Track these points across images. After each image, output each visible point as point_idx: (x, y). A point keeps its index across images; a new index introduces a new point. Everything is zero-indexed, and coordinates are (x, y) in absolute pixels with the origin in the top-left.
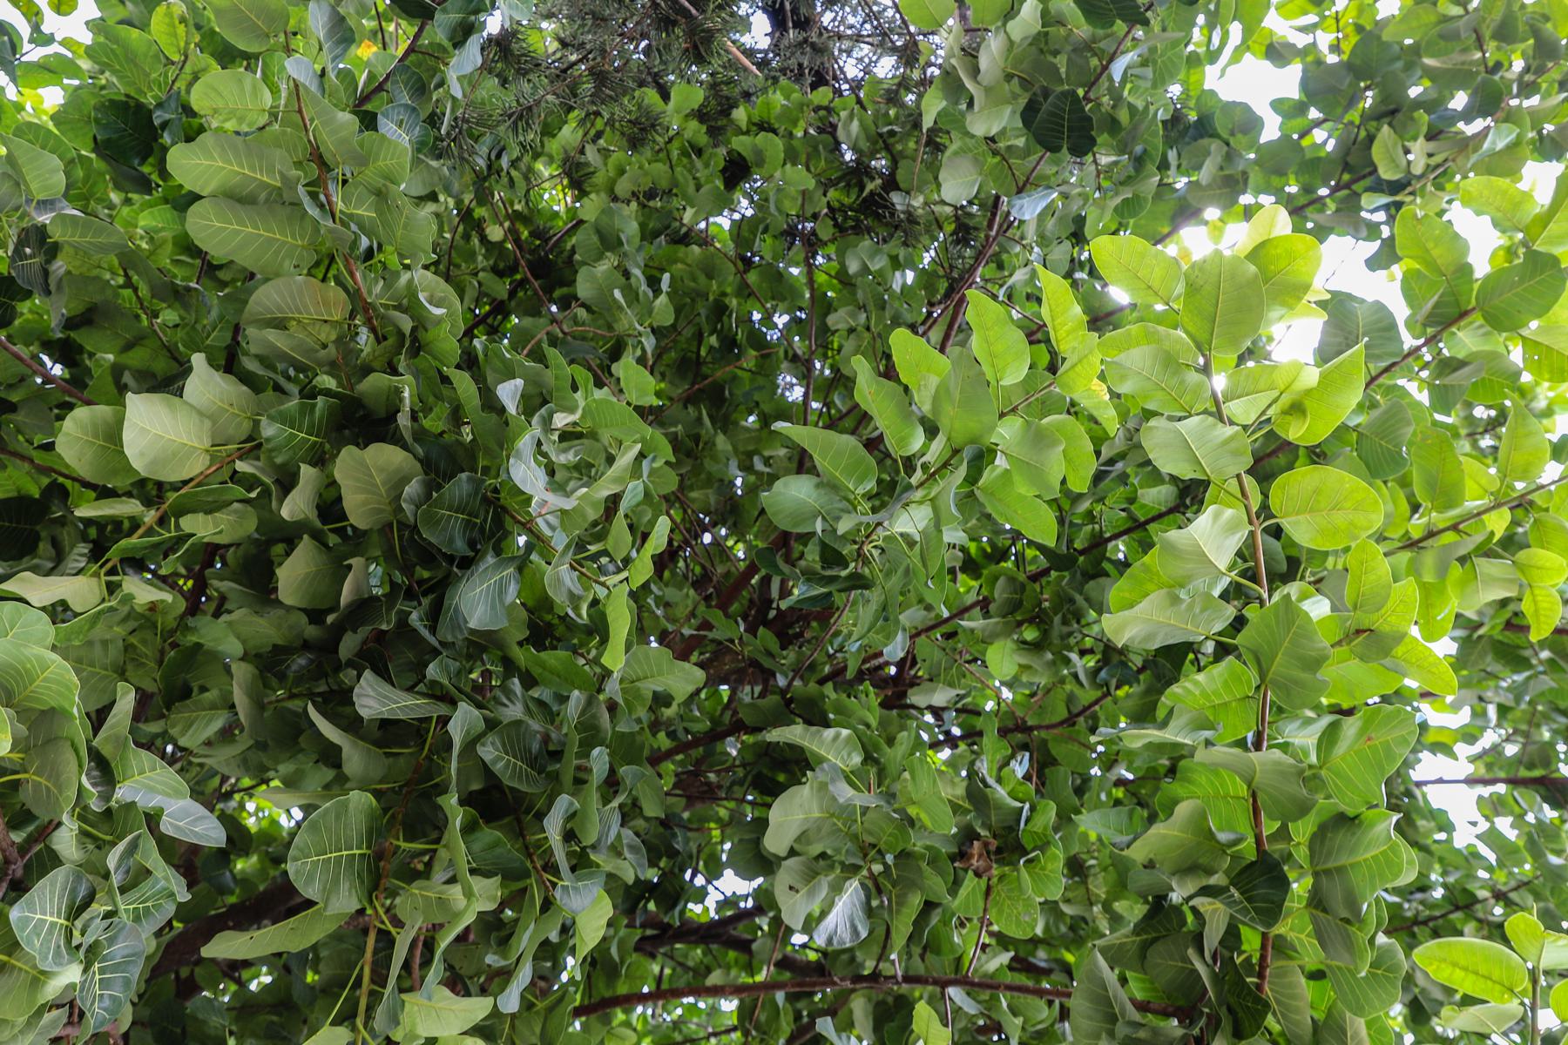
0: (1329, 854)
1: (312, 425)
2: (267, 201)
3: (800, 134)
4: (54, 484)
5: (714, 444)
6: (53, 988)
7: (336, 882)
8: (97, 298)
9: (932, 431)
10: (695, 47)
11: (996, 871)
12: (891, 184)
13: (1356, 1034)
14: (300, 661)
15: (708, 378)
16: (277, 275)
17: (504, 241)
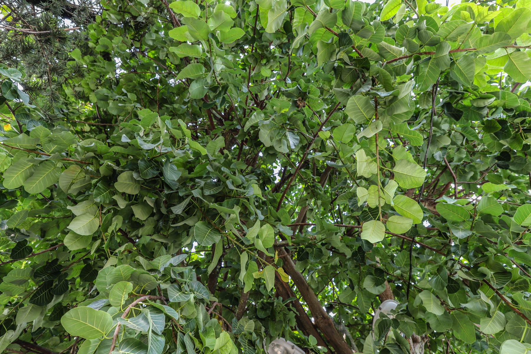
0: (348, 20)
1: (103, 190)
2: (35, 170)
3: (106, 33)
4: (84, 260)
5: (176, 108)
6: (192, 300)
7: (212, 238)
8: (40, 227)
10: (60, 38)
11: (306, 102)
12: (134, 18)
13: (385, 45)
14: (161, 223)
15: (158, 99)
16: (58, 179)
17: (91, 128)
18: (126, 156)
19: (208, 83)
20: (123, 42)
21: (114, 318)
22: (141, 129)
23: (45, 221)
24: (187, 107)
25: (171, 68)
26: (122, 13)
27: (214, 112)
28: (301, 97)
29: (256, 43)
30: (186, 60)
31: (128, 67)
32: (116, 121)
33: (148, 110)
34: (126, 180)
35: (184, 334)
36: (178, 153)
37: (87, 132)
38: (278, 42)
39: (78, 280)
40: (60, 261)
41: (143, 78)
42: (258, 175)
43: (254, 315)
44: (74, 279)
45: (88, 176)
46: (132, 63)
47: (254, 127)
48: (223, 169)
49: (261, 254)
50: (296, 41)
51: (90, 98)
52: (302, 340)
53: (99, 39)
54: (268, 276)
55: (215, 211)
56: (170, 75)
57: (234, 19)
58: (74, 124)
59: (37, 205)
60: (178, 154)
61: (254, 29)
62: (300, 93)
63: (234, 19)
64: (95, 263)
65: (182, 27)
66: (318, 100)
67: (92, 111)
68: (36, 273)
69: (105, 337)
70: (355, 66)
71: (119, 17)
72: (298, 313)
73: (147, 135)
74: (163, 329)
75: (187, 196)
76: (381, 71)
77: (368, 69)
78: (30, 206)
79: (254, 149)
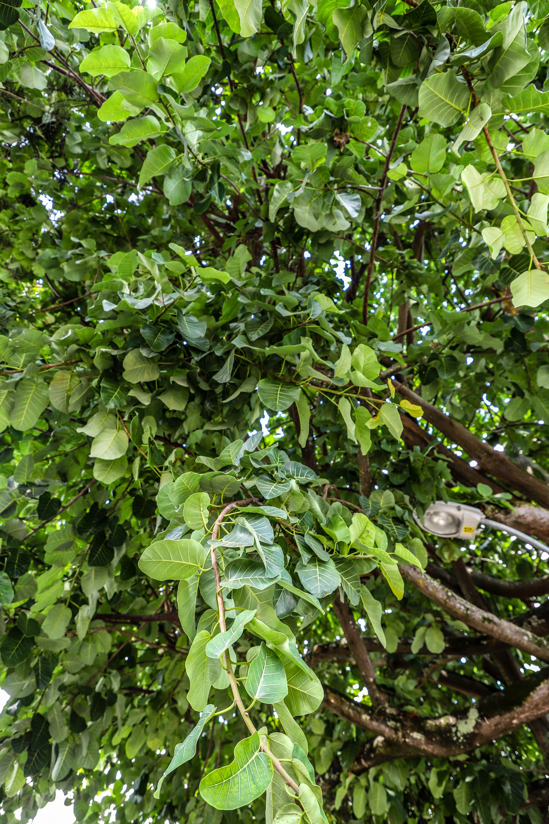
1: (113, 389)
4: (129, 493)
6: (296, 488)
8: (55, 471)
9: (147, 111)
11: (349, 134)
14: (208, 405)
15: (126, 234)
16: (48, 398)
17: (56, 317)
18: (120, 331)
19: (187, 171)
20: (41, 167)
21: (204, 543)
22: (122, 285)
23: (57, 459)
24: (172, 227)
25: (123, 177)
26: (18, 122)
27: (213, 216)
28: (337, 129)
29: (232, 72)
30: (139, 153)
31: (63, 203)
32: (84, 292)
33: (119, 254)
34: (135, 364)
35: (303, 536)
36: (189, 294)
37: (52, 324)
38: (266, 54)
39: (134, 520)
40: (100, 504)
41: (92, 210)
42: (317, 283)
43: (388, 483)
44: (127, 523)
45: (83, 379)
46: (65, 194)
47: (283, 210)
48: (263, 292)
49: (365, 391)
50: (296, 29)
51: (35, 273)
52: (469, 495)
53: (5, 179)
54: (390, 418)
55: (275, 359)
56: (128, 189)
57: (184, 44)
58: (32, 319)
59: (37, 444)
60: (190, 296)
61: (221, 50)
62: (333, 122)
63: (184, 44)
64: (145, 492)
65: (114, 93)
66: (366, 122)
67: (46, 292)
68: (79, 528)
69: (203, 570)
70: (408, 27)
71: (17, 131)
72: (449, 459)
73: (136, 290)
74: (272, 536)
75: (227, 353)
76: (459, 12)
77: (434, 23)
78: (30, 450)
79: (295, 247)
